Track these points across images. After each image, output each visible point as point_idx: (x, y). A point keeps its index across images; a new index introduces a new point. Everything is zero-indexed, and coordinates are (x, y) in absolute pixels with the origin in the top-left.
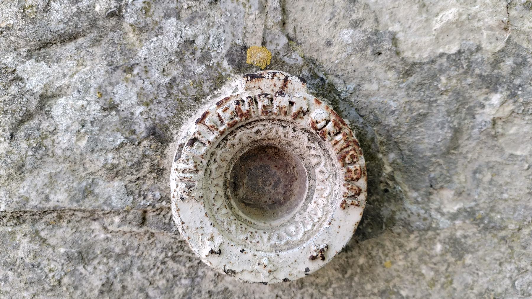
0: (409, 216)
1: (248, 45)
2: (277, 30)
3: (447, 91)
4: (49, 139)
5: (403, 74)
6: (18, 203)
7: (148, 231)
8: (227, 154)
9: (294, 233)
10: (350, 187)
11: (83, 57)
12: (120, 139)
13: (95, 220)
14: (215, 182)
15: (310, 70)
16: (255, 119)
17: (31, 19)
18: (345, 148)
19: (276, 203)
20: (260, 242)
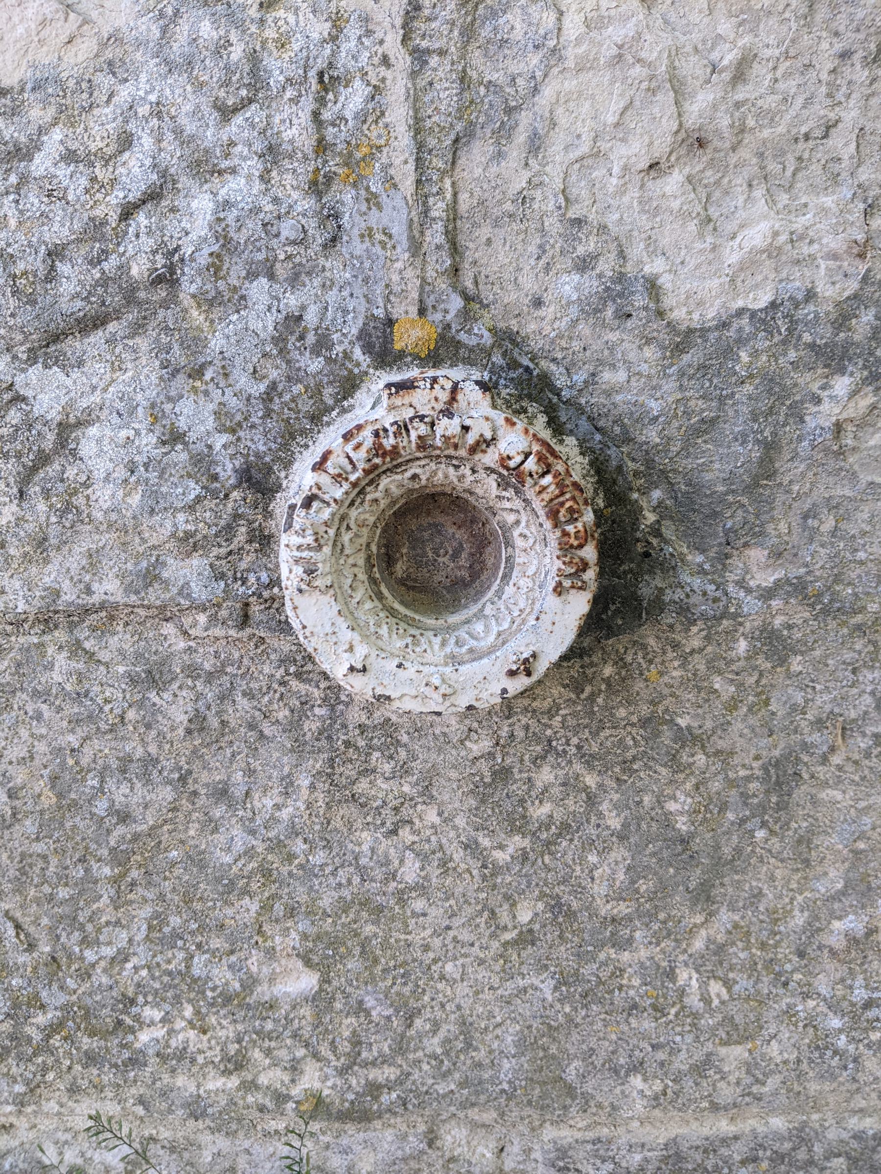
0: (688, 596)
1: (395, 317)
2: (443, 285)
3: (751, 376)
4: (80, 495)
5: (672, 351)
6: (42, 598)
7: (254, 635)
8: (367, 516)
9: (482, 635)
10: (567, 559)
11: (119, 356)
12: (194, 490)
13: (167, 620)
14: (351, 561)
15: (504, 354)
16: (408, 458)
17: (27, 296)
18: (557, 497)
19: (457, 583)
20: (428, 651)
